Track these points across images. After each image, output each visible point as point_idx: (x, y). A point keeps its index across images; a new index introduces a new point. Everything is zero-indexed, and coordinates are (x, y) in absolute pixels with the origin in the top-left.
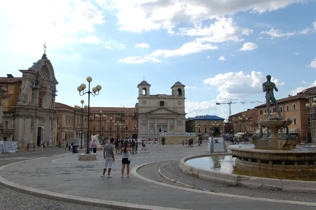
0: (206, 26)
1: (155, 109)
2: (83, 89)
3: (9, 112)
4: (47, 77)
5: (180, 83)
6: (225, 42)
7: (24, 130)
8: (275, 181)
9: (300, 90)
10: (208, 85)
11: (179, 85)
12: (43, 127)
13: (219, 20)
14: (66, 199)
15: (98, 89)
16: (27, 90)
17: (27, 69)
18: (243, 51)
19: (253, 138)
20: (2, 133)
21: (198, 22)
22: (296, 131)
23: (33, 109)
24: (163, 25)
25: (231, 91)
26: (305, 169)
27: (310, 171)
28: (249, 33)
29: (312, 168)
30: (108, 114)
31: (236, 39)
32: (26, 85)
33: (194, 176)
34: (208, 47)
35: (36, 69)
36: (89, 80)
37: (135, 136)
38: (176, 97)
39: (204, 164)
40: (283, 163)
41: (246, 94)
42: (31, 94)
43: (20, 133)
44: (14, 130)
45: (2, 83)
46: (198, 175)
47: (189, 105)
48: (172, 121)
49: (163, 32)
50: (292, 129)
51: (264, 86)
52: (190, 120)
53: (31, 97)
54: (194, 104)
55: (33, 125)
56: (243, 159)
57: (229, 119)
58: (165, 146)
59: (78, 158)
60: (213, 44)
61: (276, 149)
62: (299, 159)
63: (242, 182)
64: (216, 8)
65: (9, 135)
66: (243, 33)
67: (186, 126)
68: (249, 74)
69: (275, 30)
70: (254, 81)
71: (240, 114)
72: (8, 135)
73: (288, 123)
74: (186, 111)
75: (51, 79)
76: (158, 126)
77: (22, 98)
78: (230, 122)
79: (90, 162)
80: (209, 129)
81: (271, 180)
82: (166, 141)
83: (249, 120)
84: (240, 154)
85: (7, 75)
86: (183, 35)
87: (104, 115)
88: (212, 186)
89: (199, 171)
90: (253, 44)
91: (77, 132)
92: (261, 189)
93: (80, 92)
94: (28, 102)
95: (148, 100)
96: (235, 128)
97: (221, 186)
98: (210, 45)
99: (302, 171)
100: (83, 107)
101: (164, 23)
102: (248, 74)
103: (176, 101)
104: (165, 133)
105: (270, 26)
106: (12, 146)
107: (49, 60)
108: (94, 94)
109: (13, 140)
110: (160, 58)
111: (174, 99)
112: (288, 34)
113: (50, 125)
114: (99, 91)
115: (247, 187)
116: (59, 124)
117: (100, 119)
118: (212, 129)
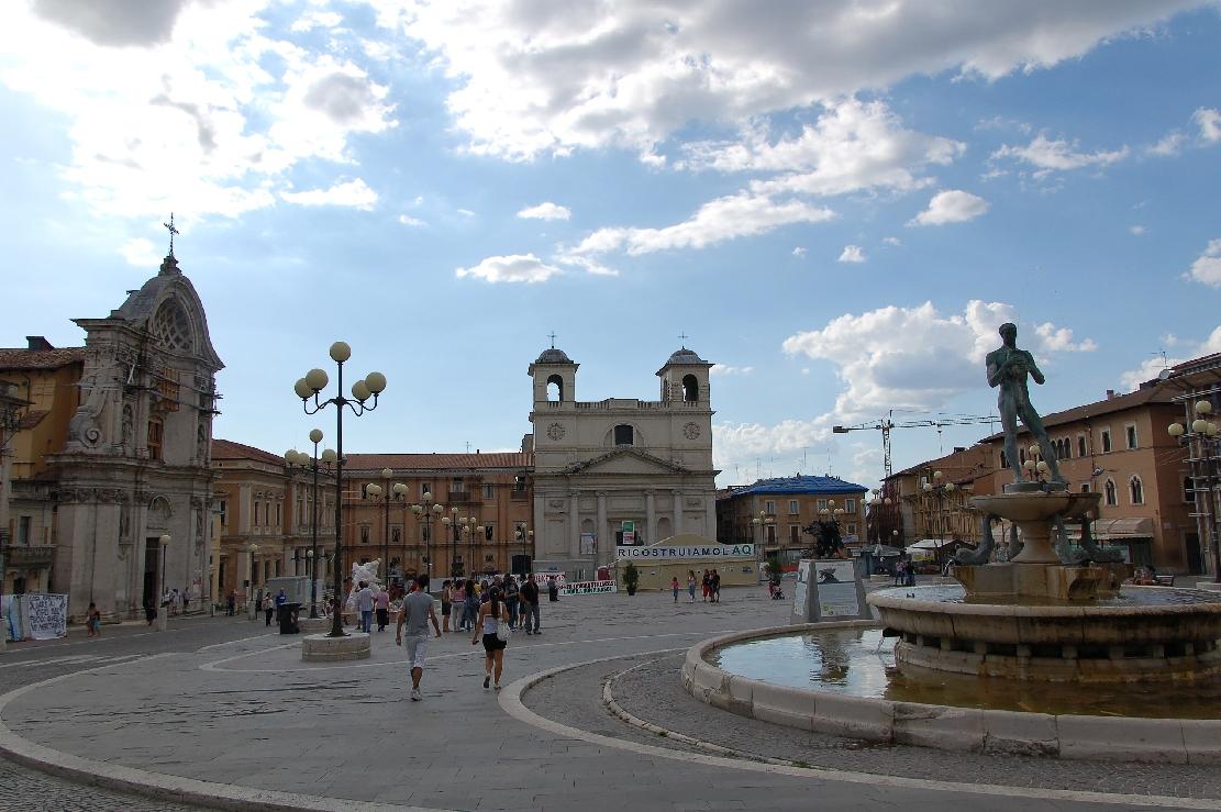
0: (786, 134)
1: (595, 455)
2: (316, 391)
3: (35, 483)
4: (181, 344)
5: (692, 353)
6: (862, 193)
7: (94, 551)
8: (1032, 722)
9: (1152, 370)
10: (802, 356)
11: (687, 359)
12: (166, 537)
13: (835, 111)
14: (253, 803)
15: (372, 387)
16: (104, 395)
17: (105, 314)
18: (932, 229)
19: (958, 563)
20: (7, 564)
21: (756, 121)
22: (1140, 528)
23: (125, 469)
24: (620, 133)
25: (889, 377)
26: (1151, 675)
27: (1170, 682)
28: (953, 156)
29: (1178, 671)
30: (418, 479)
31: (903, 180)
32: (100, 383)
33: (740, 712)
34: (796, 212)
35: (139, 314)
36: (340, 354)
37: (523, 564)
38: (676, 406)
39: (779, 664)
40: (1071, 653)
41: (950, 391)
42: (120, 408)
43: (79, 557)
44: (54, 551)
45: (9, 371)
46: (752, 706)
47: (729, 438)
48: (664, 504)
49: (621, 160)
50: (1118, 523)
51: (993, 366)
52: (735, 497)
53: (119, 421)
54: (750, 433)
55: (127, 531)
56: (920, 641)
57: (885, 489)
58: (637, 597)
59: (299, 654)
60: (815, 201)
61: (1047, 601)
62: (1130, 635)
63: (914, 730)
64: (819, 63)
65: (35, 570)
66: (928, 155)
67: (719, 518)
68: (957, 315)
69: (1049, 144)
70: (977, 341)
71: (925, 470)
72: (31, 569)
73: (1084, 500)
74: (718, 461)
75: (195, 350)
76: (609, 520)
77: (85, 426)
78: (887, 500)
79: (345, 667)
80: (805, 528)
81: (1016, 719)
82: (642, 581)
83: (958, 492)
84: (907, 624)
85: (28, 338)
86: (697, 169)
87: (400, 486)
88: (802, 746)
89: (755, 690)
90: (969, 195)
91: (296, 553)
92: (982, 753)
93: (305, 400)
94: (110, 440)
95: (568, 424)
96: (908, 526)
97: (835, 747)
98: (802, 205)
99: (1143, 682)
100: (319, 457)
101: (627, 128)
102: (951, 315)
103: (679, 424)
104: (636, 547)
105: (1029, 129)
106: (39, 614)
107: (187, 281)
108: (358, 407)
109: (51, 588)
110: (611, 257)
111: (669, 414)
112: (1102, 156)
113: (194, 530)
114: (376, 396)
115: (931, 748)
116: (226, 523)
117: (384, 501)
118: (809, 530)
